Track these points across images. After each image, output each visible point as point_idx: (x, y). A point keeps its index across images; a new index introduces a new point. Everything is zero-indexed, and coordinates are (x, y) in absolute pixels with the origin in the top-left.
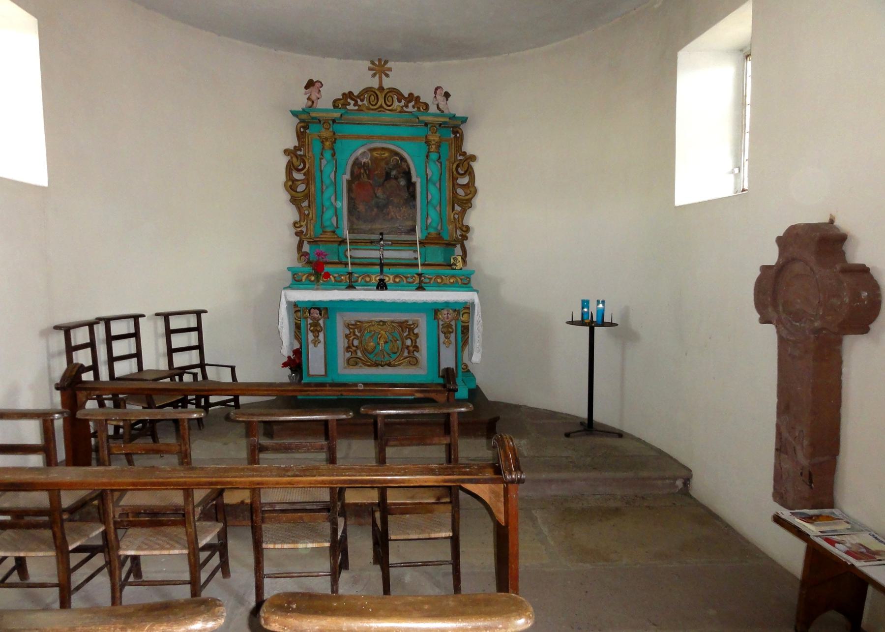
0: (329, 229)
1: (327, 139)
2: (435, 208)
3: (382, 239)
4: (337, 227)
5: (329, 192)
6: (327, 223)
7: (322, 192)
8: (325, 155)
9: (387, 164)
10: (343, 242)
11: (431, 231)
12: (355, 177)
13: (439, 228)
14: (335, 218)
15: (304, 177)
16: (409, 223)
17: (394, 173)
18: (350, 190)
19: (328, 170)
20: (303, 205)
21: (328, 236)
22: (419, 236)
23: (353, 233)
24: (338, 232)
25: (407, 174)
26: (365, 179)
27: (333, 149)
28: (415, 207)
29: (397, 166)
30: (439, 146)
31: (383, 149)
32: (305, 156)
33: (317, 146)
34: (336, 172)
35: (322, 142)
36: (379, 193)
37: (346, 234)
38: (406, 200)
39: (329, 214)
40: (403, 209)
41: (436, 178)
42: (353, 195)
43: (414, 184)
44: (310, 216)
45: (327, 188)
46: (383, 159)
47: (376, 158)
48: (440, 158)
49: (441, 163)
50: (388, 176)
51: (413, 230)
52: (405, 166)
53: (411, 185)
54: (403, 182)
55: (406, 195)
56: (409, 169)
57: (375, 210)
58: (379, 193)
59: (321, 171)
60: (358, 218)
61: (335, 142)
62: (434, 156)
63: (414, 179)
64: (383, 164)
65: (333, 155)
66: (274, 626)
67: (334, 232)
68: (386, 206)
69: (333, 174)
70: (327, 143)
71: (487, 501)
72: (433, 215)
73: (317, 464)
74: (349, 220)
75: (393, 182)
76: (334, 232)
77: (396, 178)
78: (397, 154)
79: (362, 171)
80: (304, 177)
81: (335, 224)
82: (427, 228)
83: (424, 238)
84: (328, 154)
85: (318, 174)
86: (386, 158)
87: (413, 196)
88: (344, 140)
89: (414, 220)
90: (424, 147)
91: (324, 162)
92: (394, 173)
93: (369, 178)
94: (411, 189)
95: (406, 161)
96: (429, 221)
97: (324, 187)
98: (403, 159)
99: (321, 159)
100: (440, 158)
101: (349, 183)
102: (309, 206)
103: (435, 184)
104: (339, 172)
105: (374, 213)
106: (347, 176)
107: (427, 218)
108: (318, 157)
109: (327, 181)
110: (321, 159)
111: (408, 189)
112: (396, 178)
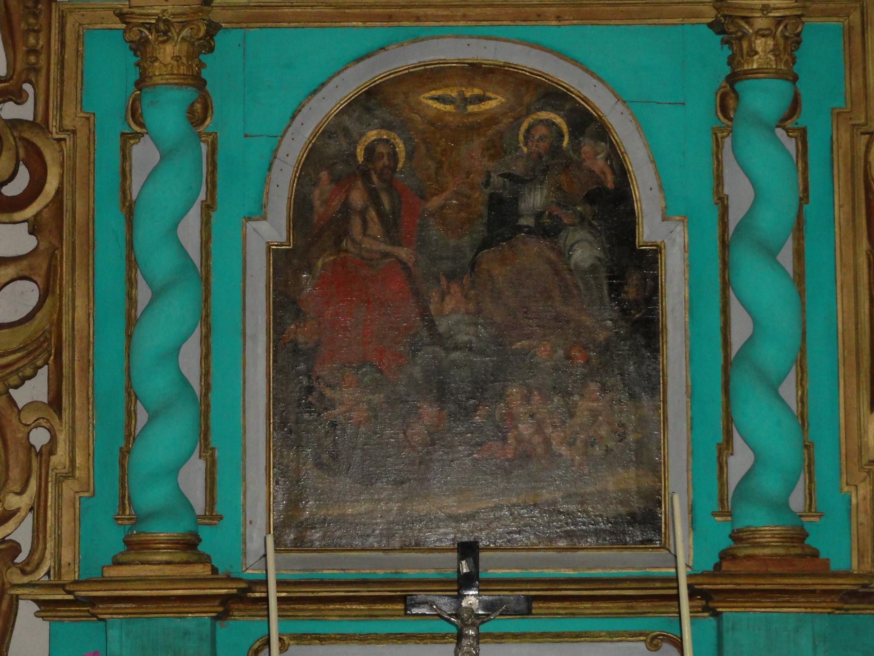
0: (164, 530)
1: (163, 28)
2: (774, 389)
3: (466, 581)
4: (212, 516)
5: (169, 322)
6: (150, 496)
7: (131, 322)
8: (153, 116)
9: (496, 149)
10: (244, 598)
11: (757, 519)
12: (314, 233)
13: (797, 501)
14: (197, 467)
15: (28, 243)
16: (620, 482)
17: (535, 199)
18: (284, 304)
19: (167, 194)
20: (22, 396)
21: (154, 571)
22: (687, 551)
23: (300, 544)
24: (211, 541)
25: (612, 206)
26: (368, 238)
27: (200, 83)
28: (653, 384)
29: (553, 162)
30: (796, 41)
31: (476, 71)
32: (40, 125)
33: (107, 69)
34: (208, 208)
35: (139, 47)
36: (452, 314)
37: (250, 543)
38: (606, 348)
39: (165, 442)
40: (590, 401)
41: (774, 220)
42: (302, 334)
43: (649, 261)
44: (60, 458)
45: (156, 295)
46: (473, 129)
47: (437, 123)
48: (795, 106)
49: (802, 136)
50: (501, 220)
51: (644, 520)
52: (599, 163)
53: (632, 268)
54: (584, 251)
55: (602, 321)
56: (622, 173)
57: (429, 411)
58: (452, 314)
59: (129, 209)
60: (330, 463)
61: (206, 43)
62: (763, 98)
63: (649, 230)
64: (472, 153)
65: (199, 114)
66: (3, 157)
67: (189, 544)
68: (485, 388)
69: (194, 216)
70: (168, 52)
71: (735, 163)
72: (765, 423)
73: (129, 197)
74: (282, 471)
75: (532, 252)
76: (189, 544)
77: (548, 230)
78: (554, 96)
79: (358, 198)
80: (28, 243)
81: (200, 506)
82: (724, 511)
83: (708, 563)
84: (167, 112)
85: (109, 223)
86: (492, 119)
87: (644, 327)
88: (255, 34)
89: (648, 458)
90: (715, 55)
91: (144, 154)
92: (535, 199)
93: (392, 227)
94: (631, 293)
95: (603, 132)
96: (739, 463)
97: (143, 294)
98: (586, 122)
99: (127, 139)
100: (795, 106)
101: (285, 265)
102: (55, 402)
103: (771, 253)
104: (231, 205)
105: (418, 431)
106: (274, 229)
107: (726, 447)
108: (111, 128)
109: (158, 261)
110: (127, 139)
111: (616, 290)
112: (548, 230)
